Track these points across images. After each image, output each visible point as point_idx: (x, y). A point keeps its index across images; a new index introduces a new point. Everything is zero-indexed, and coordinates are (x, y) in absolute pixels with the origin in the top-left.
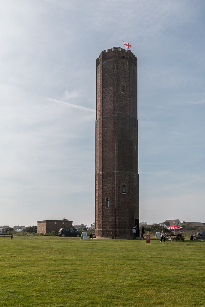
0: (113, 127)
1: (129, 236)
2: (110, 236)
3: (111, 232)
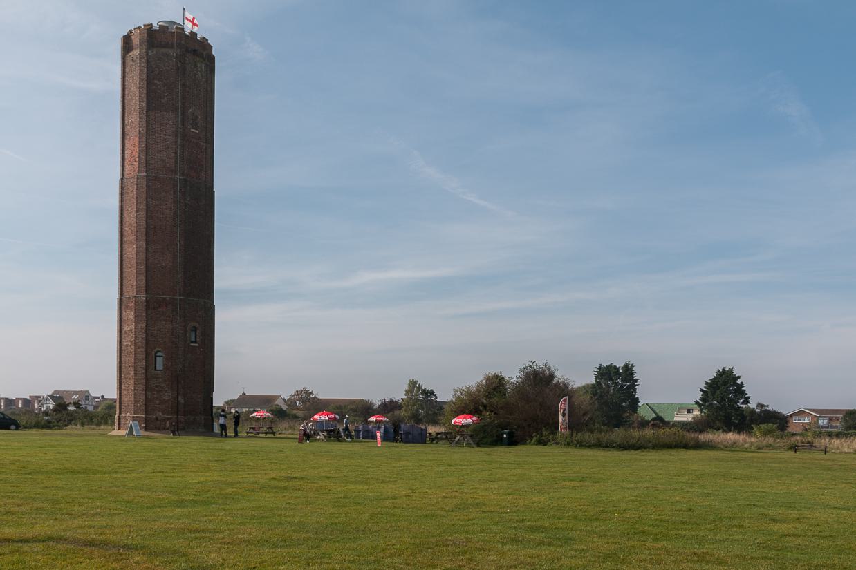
0: (175, 202)
1: (203, 430)
2: (164, 429)
3: (168, 423)
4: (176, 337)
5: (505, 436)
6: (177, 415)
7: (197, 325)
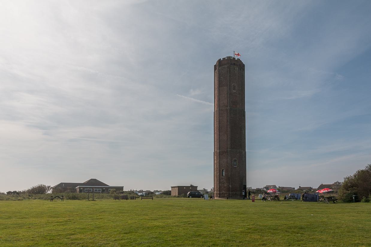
0: (227, 117)
2: (225, 197)
3: (226, 195)
4: (228, 164)
5: (354, 198)
6: (229, 192)
7: (236, 159)
